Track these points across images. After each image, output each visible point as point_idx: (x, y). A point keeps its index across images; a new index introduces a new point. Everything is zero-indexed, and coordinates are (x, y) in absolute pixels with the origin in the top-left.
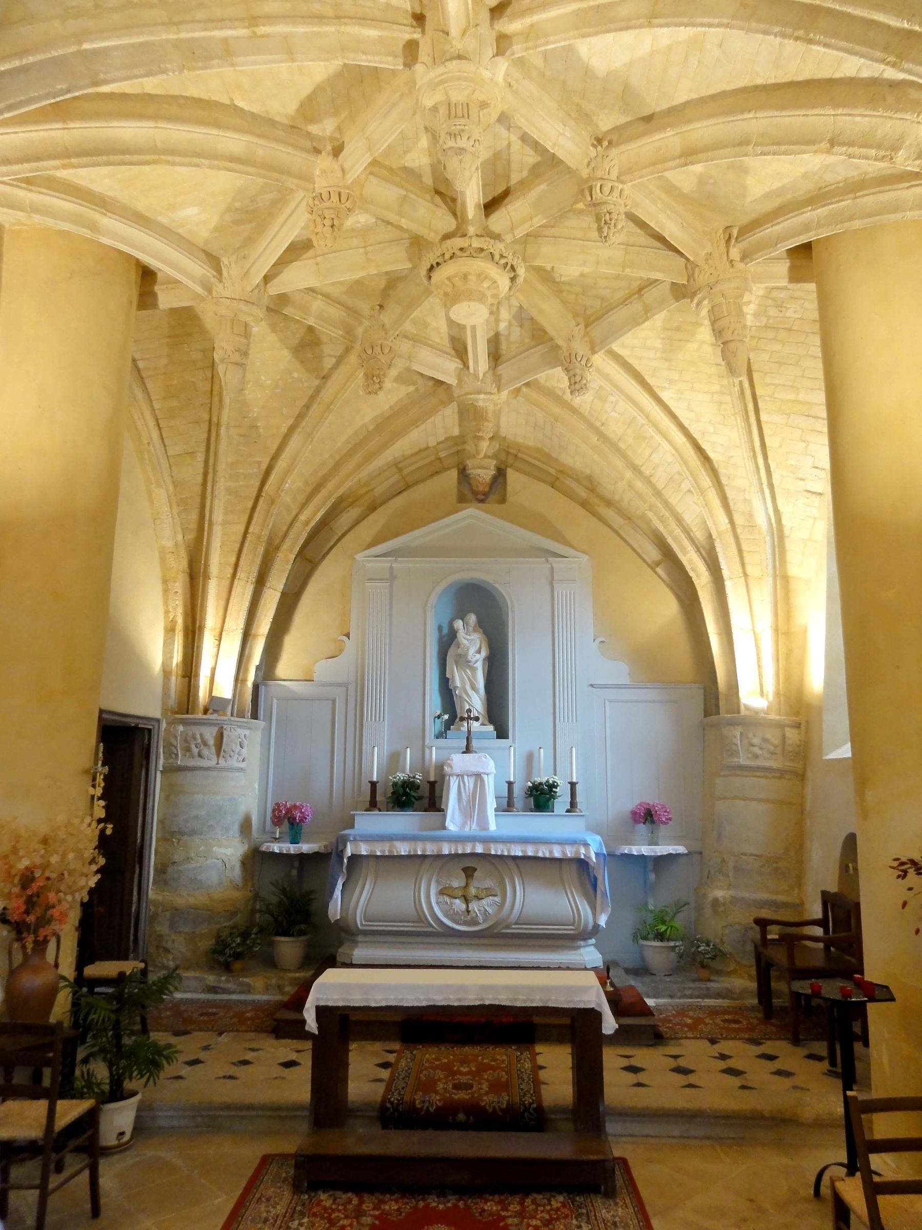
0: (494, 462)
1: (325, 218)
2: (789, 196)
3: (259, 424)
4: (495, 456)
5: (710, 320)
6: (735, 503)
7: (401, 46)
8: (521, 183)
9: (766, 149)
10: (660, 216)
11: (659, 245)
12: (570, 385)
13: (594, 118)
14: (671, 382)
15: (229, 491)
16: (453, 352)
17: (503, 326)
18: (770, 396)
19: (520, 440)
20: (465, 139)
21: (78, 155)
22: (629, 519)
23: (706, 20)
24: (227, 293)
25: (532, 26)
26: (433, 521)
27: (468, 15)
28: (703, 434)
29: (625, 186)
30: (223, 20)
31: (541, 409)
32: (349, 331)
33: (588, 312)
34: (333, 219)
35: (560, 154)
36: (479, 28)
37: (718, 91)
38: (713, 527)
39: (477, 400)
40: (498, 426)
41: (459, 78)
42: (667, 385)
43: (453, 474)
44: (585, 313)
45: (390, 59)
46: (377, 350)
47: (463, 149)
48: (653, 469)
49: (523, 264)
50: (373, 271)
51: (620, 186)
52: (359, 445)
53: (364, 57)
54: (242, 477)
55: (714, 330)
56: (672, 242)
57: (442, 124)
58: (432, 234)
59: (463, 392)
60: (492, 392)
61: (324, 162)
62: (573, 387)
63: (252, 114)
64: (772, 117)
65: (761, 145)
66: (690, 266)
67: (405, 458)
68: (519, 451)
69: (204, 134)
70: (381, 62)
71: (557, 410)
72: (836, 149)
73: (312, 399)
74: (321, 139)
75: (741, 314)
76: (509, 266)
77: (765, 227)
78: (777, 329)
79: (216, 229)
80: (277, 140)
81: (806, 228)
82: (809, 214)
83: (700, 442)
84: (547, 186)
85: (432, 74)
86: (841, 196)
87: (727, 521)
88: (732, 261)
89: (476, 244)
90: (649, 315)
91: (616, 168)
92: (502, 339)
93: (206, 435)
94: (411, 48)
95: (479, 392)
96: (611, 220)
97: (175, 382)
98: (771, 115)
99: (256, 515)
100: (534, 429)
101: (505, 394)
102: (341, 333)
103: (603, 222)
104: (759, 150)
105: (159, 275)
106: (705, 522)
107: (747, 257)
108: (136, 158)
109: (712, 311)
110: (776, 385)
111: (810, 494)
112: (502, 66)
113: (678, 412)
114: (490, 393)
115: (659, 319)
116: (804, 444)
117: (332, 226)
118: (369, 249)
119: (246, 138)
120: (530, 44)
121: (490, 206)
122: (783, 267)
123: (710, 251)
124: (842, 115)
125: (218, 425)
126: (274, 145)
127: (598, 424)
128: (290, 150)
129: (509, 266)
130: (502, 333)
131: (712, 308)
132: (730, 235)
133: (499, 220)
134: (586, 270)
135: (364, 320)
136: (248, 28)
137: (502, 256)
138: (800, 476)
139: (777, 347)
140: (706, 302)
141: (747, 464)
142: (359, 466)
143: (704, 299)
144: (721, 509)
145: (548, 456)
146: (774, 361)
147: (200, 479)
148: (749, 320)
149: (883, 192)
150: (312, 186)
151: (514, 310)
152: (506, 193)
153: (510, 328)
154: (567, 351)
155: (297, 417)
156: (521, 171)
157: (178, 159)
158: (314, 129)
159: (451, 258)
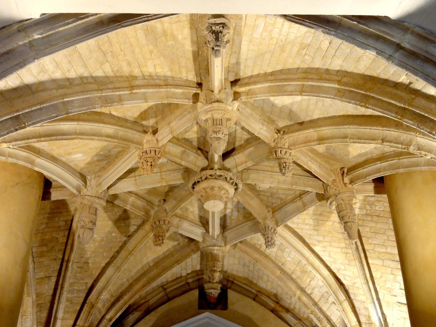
0: (220, 286)
1: (148, 162)
2: (370, 156)
3: (89, 261)
4: (220, 282)
5: (337, 211)
6: (359, 310)
7: (191, 95)
8: (241, 146)
9: (355, 141)
10: (309, 163)
11: (309, 175)
12: (266, 242)
13: (276, 122)
14: (319, 241)
15: (68, 300)
16: (200, 224)
17: (228, 211)
18: (373, 250)
19: (235, 273)
20: (220, 134)
21: (44, 136)
22: (300, 320)
23: (324, 95)
24: (89, 193)
25: (249, 90)
26: (185, 320)
27: (222, 86)
28: (339, 270)
29: (292, 151)
30: (119, 88)
31: (248, 255)
32: (147, 213)
33: (274, 205)
34: (151, 162)
35: (261, 137)
36: (226, 89)
37: (332, 115)
38: (348, 323)
39: (213, 250)
40: (223, 265)
41: (218, 110)
42: (317, 243)
43: (196, 293)
44: (272, 205)
45: (187, 100)
46: (162, 222)
47: (219, 138)
48: (312, 290)
49: (241, 183)
50: (164, 184)
51: (290, 151)
52: (144, 274)
53: (176, 100)
54: (76, 291)
55: (339, 216)
56: (315, 175)
57: (210, 127)
58: (196, 168)
59: (205, 245)
60: (222, 245)
61: (149, 137)
62: (267, 244)
63: (119, 118)
64: (356, 128)
65: (352, 138)
66: (325, 186)
67: (168, 283)
68: (234, 279)
69: (98, 126)
70: (183, 102)
71: (257, 256)
72: (385, 143)
73: (121, 248)
74: (147, 127)
75: (352, 209)
76: (234, 184)
77: (359, 169)
78: (372, 216)
79: (89, 163)
80: (127, 128)
81: (379, 171)
82: (379, 165)
83: (337, 274)
84: (254, 148)
85: (206, 107)
86: (393, 158)
87: (356, 320)
88: (345, 184)
89: (218, 173)
90: (306, 208)
91: (287, 143)
92: (228, 218)
93: (58, 267)
94: (196, 97)
95: (214, 246)
96: (286, 166)
97: (47, 237)
98: (356, 127)
99: (82, 314)
100: (244, 266)
101: (228, 247)
102: (143, 213)
103: (282, 167)
104: (352, 141)
105: (54, 184)
106: (344, 321)
107: (353, 182)
108: (68, 137)
109: (337, 207)
110: (375, 244)
111: (400, 304)
112: (236, 104)
113: (324, 258)
114: (221, 246)
115: (311, 210)
116: (394, 276)
117: (151, 165)
118: (163, 173)
119: (116, 127)
120: (249, 97)
121: (226, 155)
122: (371, 187)
123: (334, 179)
124: (386, 130)
125: (68, 261)
126: (127, 130)
127: (280, 264)
128: (134, 132)
129: (234, 184)
130: (228, 215)
131: (338, 205)
132: (343, 171)
133: (229, 162)
134: (272, 185)
135: (155, 207)
136: (129, 91)
137: (231, 179)
138: (394, 294)
139: (373, 225)
140: (334, 203)
141: (364, 287)
142: (144, 286)
143: (333, 201)
144: (352, 313)
145: (251, 282)
146: (372, 231)
147: (51, 292)
148: (357, 211)
149: (411, 158)
150: (142, 147)
151: (235, 203)
152: (233, 150)
153: (232, 212)
154: (264, 224)
155: (111, 258)
156: (241, 141)
157: (85, 137)
158: (145, 123)
159: (205, 179)
